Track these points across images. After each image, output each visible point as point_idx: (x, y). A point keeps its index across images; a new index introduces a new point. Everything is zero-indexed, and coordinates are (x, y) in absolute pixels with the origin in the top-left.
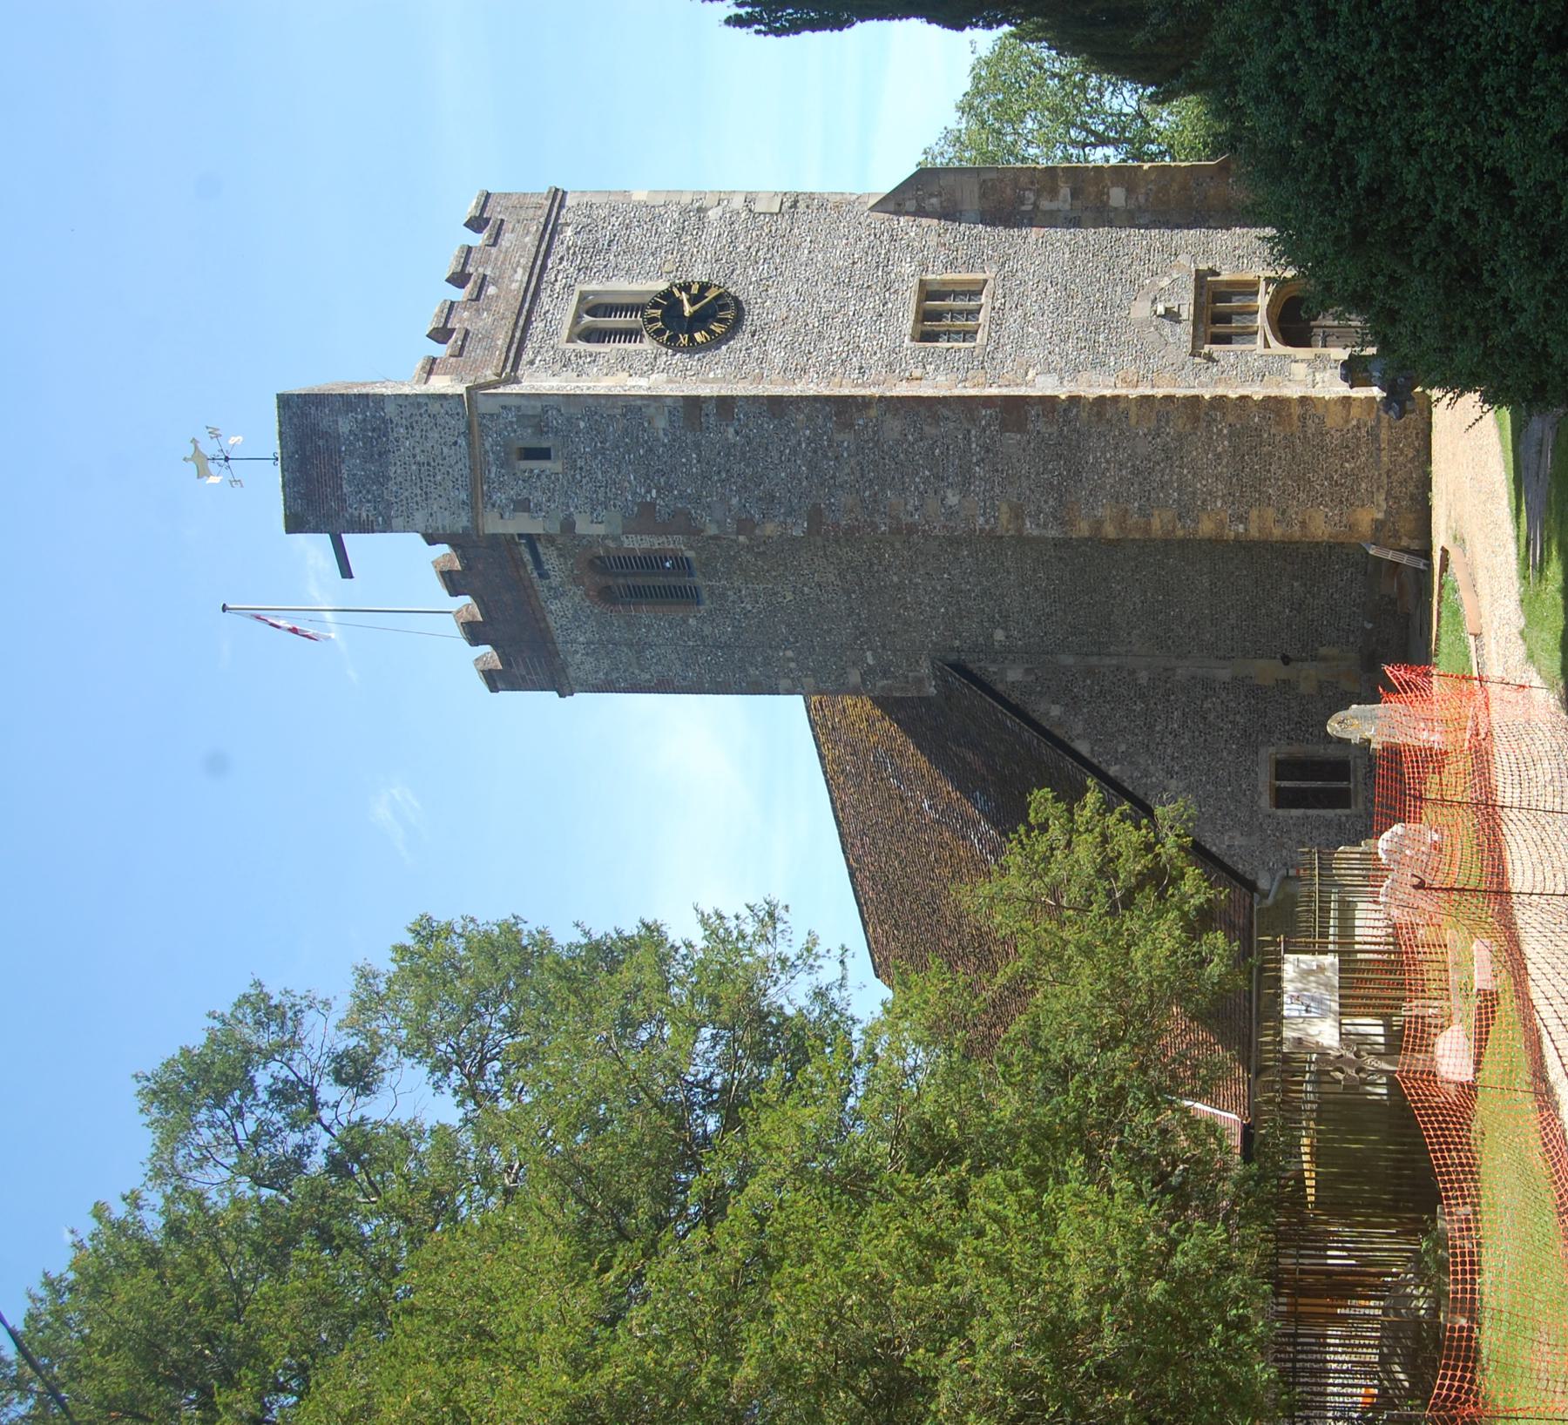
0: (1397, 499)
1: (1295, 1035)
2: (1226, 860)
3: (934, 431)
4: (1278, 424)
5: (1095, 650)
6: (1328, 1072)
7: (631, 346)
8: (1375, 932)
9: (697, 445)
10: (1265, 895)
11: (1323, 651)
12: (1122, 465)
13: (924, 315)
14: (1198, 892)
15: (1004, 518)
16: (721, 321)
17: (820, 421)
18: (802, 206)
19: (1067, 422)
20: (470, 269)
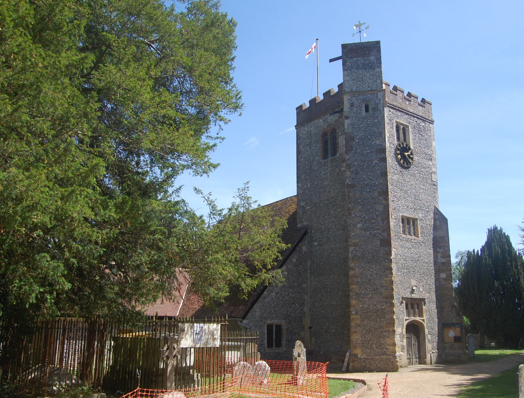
0: (364, 362)
1: (186, 329)
2: (252, 310)
3: (379, 220)
4: (386, 323)
5: (312, 271)
6: (167, 343)
7: (396, 138)
8: (230, 359)
9: (372, 152)
10: (241, 322)
11: (313, 339)
12: (371, 276)
13: (408, 219)
14: (247, 286)
15: (354, 241)
16: (404, 162)
17: (380, 187)
18: (434, 187)
19: (384, 259)
20: (412, 98)
